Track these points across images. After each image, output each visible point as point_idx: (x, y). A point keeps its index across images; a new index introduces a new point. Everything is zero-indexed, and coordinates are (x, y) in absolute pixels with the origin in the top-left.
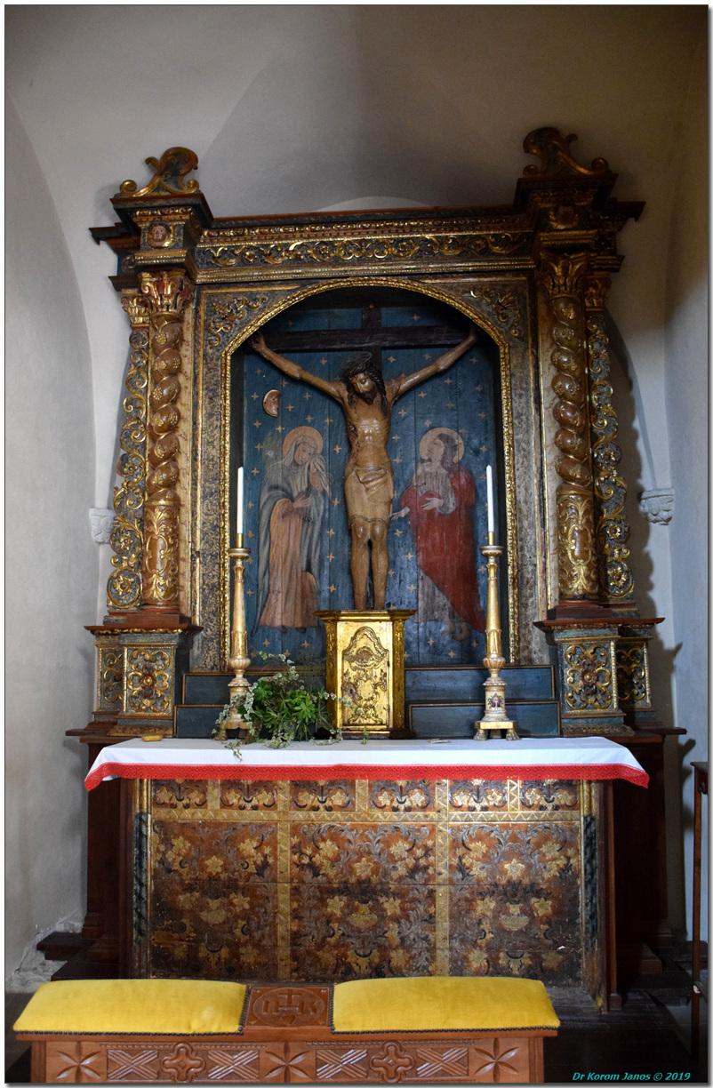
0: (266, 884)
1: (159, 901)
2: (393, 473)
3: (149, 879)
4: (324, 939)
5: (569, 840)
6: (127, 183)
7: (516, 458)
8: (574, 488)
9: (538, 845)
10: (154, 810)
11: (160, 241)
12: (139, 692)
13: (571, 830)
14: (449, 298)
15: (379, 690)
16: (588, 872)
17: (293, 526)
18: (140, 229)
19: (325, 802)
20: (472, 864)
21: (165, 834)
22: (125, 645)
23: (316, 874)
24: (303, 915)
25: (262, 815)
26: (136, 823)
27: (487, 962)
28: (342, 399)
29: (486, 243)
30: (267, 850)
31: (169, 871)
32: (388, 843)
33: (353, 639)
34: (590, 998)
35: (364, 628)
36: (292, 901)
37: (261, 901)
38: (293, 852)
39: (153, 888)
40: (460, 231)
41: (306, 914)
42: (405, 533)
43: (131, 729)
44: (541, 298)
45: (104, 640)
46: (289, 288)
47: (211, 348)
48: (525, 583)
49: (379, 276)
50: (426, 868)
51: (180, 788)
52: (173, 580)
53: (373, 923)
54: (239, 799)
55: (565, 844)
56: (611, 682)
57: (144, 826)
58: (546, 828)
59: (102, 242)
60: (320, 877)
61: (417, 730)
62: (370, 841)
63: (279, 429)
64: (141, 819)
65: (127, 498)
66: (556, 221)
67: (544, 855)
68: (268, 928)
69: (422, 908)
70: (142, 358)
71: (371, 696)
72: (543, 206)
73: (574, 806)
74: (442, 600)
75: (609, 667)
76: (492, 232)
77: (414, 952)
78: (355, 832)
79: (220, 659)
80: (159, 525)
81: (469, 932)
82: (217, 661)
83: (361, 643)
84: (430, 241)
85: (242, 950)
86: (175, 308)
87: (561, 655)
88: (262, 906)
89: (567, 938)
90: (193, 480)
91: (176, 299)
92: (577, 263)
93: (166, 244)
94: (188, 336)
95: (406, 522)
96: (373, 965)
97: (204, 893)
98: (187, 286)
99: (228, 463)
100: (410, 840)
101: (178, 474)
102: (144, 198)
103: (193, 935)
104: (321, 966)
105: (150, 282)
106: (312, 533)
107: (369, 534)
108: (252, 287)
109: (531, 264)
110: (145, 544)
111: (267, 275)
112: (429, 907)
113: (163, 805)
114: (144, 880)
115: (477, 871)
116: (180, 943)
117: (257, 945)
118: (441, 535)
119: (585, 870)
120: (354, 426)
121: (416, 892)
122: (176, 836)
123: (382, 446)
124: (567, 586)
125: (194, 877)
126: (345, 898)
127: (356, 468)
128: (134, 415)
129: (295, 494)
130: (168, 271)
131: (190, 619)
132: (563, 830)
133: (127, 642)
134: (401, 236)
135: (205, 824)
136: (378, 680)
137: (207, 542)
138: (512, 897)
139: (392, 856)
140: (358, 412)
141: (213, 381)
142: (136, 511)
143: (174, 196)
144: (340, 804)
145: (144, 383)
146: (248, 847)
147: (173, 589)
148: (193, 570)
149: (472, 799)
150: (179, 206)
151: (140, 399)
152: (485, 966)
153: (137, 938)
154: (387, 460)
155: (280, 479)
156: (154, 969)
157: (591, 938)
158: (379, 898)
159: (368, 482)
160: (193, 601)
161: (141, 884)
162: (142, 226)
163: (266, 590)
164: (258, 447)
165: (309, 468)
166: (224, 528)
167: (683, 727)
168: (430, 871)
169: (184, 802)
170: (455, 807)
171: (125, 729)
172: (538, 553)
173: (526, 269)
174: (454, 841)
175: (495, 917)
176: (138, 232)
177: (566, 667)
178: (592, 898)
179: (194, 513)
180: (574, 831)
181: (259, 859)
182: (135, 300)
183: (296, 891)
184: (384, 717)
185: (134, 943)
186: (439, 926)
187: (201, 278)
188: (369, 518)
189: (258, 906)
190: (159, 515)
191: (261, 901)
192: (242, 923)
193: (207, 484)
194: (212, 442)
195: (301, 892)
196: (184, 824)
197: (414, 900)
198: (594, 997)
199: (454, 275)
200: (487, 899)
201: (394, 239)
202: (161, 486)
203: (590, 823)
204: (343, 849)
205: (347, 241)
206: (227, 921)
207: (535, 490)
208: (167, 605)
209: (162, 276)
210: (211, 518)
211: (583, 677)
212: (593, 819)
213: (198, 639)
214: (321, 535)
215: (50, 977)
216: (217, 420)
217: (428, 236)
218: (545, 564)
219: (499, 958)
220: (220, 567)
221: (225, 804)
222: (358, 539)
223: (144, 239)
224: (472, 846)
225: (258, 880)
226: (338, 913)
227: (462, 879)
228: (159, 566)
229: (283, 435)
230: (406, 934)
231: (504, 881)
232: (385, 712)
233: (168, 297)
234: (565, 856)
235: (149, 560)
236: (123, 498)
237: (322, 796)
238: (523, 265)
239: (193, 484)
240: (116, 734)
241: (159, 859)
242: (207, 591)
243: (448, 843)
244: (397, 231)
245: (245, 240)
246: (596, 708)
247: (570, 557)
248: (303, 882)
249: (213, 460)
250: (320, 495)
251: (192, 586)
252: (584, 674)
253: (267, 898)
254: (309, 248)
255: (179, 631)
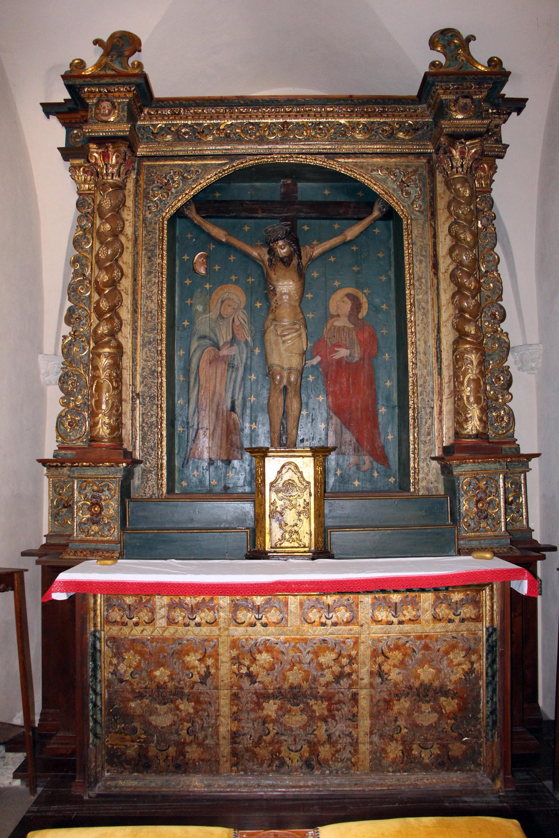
0: (208, 691)
1: (112, 707)
2: (306, 327)
3: (103, 688)
4: (260, 738)
5: (472, 647)
6: (77, 61)
7: (417, 315)
8: (469, 342)
9: (447, 653)
10: (107, 628)
11: (106, 115)
12: (88, 519)
13: (475, 639)
14: (360, 175)
15: (302, 517)
16: (489, 674)
17: (219, 371)
18: (87, 104)
19: (261, 619)
20: (390, 670)
21: (118, 649)
22: (75, 478)
23: (253, 682)
24: (241, 717)
25: (205, 630)
26: (91, 639)
27: (403, 753)
28: (263, 261)
29: (392, 129)
30: (210, 662)
31: (121, 681)
32: (316, 654)
33: (279, 472)
34: (490, 781)
35: (290, 463)
36: (232, 705)
37: (204, 706)
38: (232, 663)
39: (106, 697)
40: (369, 117)
41: (244, 716)
42: (316, 380)
43: (81, 552)
44: (439, 178)
45: (54, 471)
46: (220, 162)
47: (150, 213)
48: (424, 423)
49: (299, 154)
50: (349, 675)
51: (130, 609)
52: (117, 420)
53: (304, 723)
54: (184, 617)
55: (469, 651)
56: (500, 509)
57: (98, 642)
58: (454, 637)
59: (51, 116)
60: (256, 684)
61: (334, 552)
62: (301, 652)
63: (207, 286)
64: (95, 636)
65: (74, 345)
66: (455, 111)
67: (452, 661)
68: (210, 729)
69: (346, 709)
70: (87, 220)
71: (295, 522)
72: (444, 97)
73: (478, 619)
74: (348, 436)
75: (499, 497)
76: (396, 120)
77: (339, 746)
78: (287, 645)
79: (158, 489)
80: (104, 370)
81: (387, 729)
82: (155, 491)
83: (287, 476)
84: (344, 125)
85: (188, 749)
86: (119, 176)
87: (459, 486)
88: (204, 710)
89: (471, 730)
90: (133, 330)
91: (120, 168)
92: (472, 149)
93: (112, 119)
94: (130, 203)
95: (317, 369)
96: (304, 758)
97: (153, 700)
98: (129, 157)
99: (165, 316)
100: (336, 650)
101: (121, 325)
102: (92, 76)
103: (143, 736)
104: (258, 761)
105: (97, 153)
106: (236, 378)
107: (285, 382)
108: (187, 160)
109: (430, 149)
110: (92, 386)
111: (200, 150)
112: (353, 707)
113: (115, 623)
114: (98, 690)
115: (395, 675)
116: (132, 743)
117: (200, 745)
118: (348, 380)
119: (487, 673)
120: (273, 285)
121: (341, 695)
122: (127, 650)
123: (297, 304)
124: (463, 427)
125: (144, 686)
126: (278, 702)
127: (275, 323)
128: (80, 271)
129: (221, 344)
130: (113, 143)
131: (131, 453)
132: (468, 640)
133: (76, 475)
134: (318, 120)
135: (153, 640)
136: (301, 509)
137: (146, 385)
138: (424, 697)
139: (320, 665)
140: (277, 273)
141: (151, 243)
142: (82, 357)
143: (120, 75)
144: (275, 621)
145: (89, 243)
146: (192, 659)
147: (117, 427)
148: (133, 410)
149: (390, 614)
150: (123, 84)
151: (86, 257)
152: (400, 756)
153: (93, 741)
154: (301, 316)
155: (208, 330)
156: (109, 767)
157: (491, 730)
158: (309, 701)
159: (284, 336)
160: (134, 438)
161: (96, 693)
162: (90, 102)
163: (196, 427)
164: (189, 302)
165: (233, 321)
166: (161, 373)
167: (554, 545)
168: (354, 677)
169: (134, 619)
170: (375, 621)
171: (76, 552)
172: (436, 397)
173: (426, 153)
174: (375, 650)
175: (410, 715)
176: (86, 107)
177: (462, 496)
178: (492, 696)
179: (134, 360)
180: (478, 640)
181: (203, 670)
182: (82, 169)
183: (235, 697)
184: (306, 540)
185: (91, 746)
186: (361, 723)
187: (141, 151)
188: (286, 367)
189: (201, 710)
190: (104, 362)
191: (204, 706)
192: (187, 725)
193: (146, 334)
194: (151, 297)
195: (240, 698)
196: (134, 640)
197: (340, 702)
198: (493, 780)
199: (364, 155)
200: (402, 700)
201: (312, 123)
202: (105, 334)
203: (492, 633)
204: (277, 659)
205: (271, 123)
206: (174, 723)
207: (432, 342)
208: (112, 441)
209: (107, 148)
210: (149, 363)
211: (477, 505)
212: (494, 630)
213: (138, 470)
214: (243, 379)
215: (12, 776)
216: (155, 277)
217: (342, 121)
218: (441, 407)
219: (413, 750)
220: (158, 407)
221: (171, 622)
222: (275, 385)
223: (91, 114)
224: (389, 654)
225: (202, 688)
226: (274, 716)
227: (382, 683)
228: (104, 407)
229: (211, 292)
230: (332, 731)
231: (417, 684)
232: (307, 537)
233: (113, 166)
234: (470, 661)
235: (96, 401)
236: (70, 345)
237: (259, 613)
238: (423, 149)
239: (133, 334)
240: (68, 557)
241: (112, 671)
242: (146, 429)
243: (369, 652)
244: (315, 116)
245: (181, 119)
246: (487, 532)
247: (466, 402)
248: (241, 688)
249: (151, 312)
250: (243, 344)
251: (133, 425)
252: (477, 502)
253: (210, 703)
254: (238, 128)
255: (124, 465)
